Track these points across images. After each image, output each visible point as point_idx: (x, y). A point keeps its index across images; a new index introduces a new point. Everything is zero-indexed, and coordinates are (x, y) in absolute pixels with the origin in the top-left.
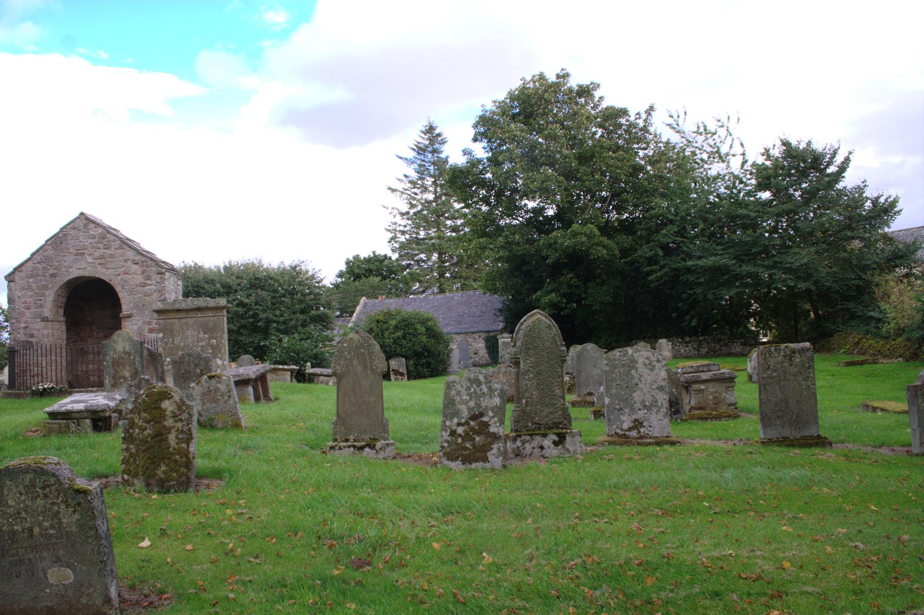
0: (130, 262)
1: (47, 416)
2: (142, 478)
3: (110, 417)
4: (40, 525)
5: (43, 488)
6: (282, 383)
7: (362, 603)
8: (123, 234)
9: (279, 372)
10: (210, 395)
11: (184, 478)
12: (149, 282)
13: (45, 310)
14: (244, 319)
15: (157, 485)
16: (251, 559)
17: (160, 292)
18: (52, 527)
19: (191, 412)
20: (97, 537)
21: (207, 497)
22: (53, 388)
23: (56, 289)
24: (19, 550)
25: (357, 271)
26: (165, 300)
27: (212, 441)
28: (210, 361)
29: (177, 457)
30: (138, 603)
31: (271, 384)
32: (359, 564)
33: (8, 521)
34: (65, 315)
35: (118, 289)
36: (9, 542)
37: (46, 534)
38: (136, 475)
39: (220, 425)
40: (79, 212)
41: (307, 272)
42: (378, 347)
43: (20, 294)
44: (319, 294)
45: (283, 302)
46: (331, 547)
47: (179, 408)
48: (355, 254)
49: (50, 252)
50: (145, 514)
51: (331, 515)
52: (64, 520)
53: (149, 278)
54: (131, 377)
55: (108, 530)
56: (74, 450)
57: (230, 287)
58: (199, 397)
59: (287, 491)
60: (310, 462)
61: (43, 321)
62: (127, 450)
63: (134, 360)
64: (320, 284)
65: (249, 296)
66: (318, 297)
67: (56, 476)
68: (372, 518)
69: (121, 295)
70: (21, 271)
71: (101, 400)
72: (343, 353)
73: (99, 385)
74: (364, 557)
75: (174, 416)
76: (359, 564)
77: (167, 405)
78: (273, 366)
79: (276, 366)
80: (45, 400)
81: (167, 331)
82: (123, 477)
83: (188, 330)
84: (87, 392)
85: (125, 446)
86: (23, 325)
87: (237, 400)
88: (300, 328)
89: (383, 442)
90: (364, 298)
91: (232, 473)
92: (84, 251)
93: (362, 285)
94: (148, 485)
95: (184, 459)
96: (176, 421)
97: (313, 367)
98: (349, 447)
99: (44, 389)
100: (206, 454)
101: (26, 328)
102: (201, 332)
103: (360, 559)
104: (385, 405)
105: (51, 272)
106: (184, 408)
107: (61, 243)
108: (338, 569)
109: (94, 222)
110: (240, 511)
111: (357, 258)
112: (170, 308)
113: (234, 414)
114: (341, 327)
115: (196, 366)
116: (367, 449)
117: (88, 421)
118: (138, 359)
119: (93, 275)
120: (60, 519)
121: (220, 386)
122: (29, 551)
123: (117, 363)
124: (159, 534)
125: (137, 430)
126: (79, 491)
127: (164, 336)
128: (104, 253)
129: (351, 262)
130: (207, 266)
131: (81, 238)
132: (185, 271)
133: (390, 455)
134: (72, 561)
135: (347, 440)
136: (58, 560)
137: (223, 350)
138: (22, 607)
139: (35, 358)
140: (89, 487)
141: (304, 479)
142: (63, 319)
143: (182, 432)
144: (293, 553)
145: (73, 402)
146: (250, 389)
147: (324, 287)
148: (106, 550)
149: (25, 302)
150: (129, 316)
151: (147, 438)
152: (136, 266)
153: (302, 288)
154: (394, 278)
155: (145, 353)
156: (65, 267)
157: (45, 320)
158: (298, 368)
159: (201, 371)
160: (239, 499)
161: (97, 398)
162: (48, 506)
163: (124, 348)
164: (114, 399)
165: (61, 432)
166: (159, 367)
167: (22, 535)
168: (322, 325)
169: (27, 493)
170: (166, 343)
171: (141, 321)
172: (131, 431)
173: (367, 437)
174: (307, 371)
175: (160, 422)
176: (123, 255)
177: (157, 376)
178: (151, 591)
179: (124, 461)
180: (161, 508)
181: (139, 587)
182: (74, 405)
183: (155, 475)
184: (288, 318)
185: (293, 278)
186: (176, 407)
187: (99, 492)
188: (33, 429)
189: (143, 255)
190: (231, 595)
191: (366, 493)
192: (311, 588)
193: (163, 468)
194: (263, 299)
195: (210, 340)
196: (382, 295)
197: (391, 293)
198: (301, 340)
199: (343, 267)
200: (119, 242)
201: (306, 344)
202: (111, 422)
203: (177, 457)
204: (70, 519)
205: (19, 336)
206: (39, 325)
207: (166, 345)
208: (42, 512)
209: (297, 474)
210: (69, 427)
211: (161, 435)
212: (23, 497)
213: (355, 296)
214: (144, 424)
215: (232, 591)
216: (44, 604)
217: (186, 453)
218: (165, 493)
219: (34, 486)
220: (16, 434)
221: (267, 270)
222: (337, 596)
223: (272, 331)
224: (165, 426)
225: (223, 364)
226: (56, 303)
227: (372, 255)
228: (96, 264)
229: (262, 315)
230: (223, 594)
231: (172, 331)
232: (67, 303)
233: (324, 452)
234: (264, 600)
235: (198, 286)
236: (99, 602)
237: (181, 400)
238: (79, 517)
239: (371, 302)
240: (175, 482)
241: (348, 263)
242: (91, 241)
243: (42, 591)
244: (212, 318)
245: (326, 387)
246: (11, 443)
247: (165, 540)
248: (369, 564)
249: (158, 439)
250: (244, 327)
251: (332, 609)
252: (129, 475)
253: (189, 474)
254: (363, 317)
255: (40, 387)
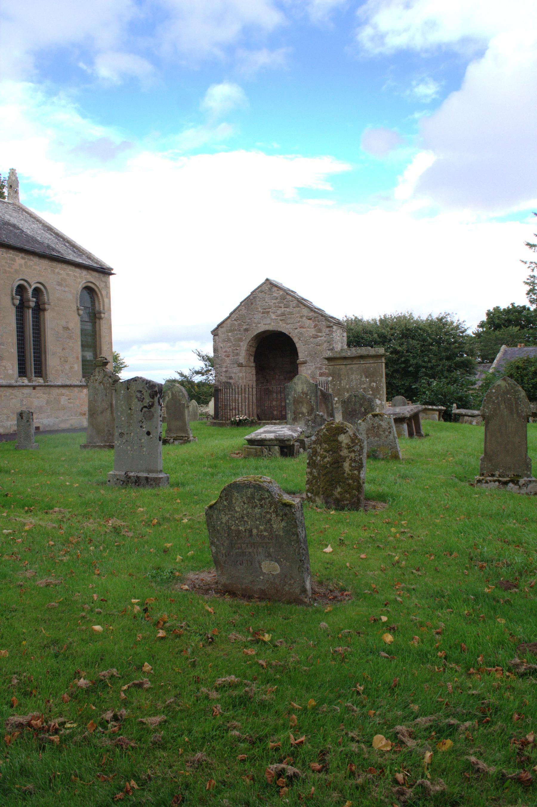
0: (305, 318)
1: (246, 442)
2: (322, 496)
3: (293, 445)
4: (257, 528)
5: (260, 500)
6: (431, 421)
7: (511, 620)
8: (299, 294)
9: (428, 412)
10: (374, 430)
11: (355, 499)
12: (320, 334)
13: (240, 357)
14: (397, 365)
15: (334, 503)
16: (414, 571)
17: (329, 342)
18: (266, 530)
19: (362, 445)
20: (298, 541)
21: (374, 516)
22: (246, 419)
23: (248, 341)
24: (243, 545)
25: (497, 321)
26: (332, 349)
27: (375, 469)
28: (373, 401)
29: (350, 481)
30: (325, 596)
31: (422, 422)
32: (508, 586)
33: (235, 522)
34: (255, 361)
35: (295, 340)
36: (236, 538)
37: (261, 535)
38: (317, 494)
39: (381, 456)
40: (265, 279)
41: (452, 323)
42: (523, 393)
43: (222, 345)
44: (462, 343)
45: (431, 350)
46: (482, 568)
47: (353, 441)
48: (495, 306)
49: (244, 312)
50: (327, 526)
51: (481, 540)
52: (274, 526)
53: (320, 331)
54: (308, 413)
55: (305, 536)
56: (268, 470)
57: (385, 337)
58: (365, 432)
59: (442, 516)
60: (460, 492)
61: (239, 366)
62: (311, 473)
63: (310, 399)
64: (464, 334)
65: (401, 345)
66: (462, 346)
67: (270, 492)
68: (518, 546)
69: (297, 345)
70: (223, 327)
71: (287, 432)
72: (491, 398)
73: (282, 418)
74: (511, 580)
75: (349, 447)
76: (508, 586)
77: (343, 438)
78: (424, 407)
79: (426, 406)
80: (241, 429)
81: (336, 375)
82: (307, 495)
83: (352, 374)
84: (272, 424)
85: (309, 470)
86: (224, 370)
87: (396, 435)
88: (446, 373)
89: (526, 479)
90: (504, 347)
91: (394, 497)
92: (269, 310)
93: (502, 334)
94: (327, 503)
95: (356, 483)
96: (350, 452)
97: (458, 408)
98: (495, 481)
99: (240, 420)
100: (372, 480)
101: (226, 371)
102: (363, 376)
103: (508, 581)
104: (529, 445)
105: (245, 327)
106: (357, 441)
107: (252, 304)
108: (489, 588)
109: (276, 286)
110: (402, 530)
111: (497, 309)
112: (338, 356)
113: (394, 447)
114: (482, 372)
115: (361, 405)
116: (511, 485)
117: (277, 447)
118: (313, 398)
119: (276, 329)
120: (271, 525)
121: (382, 423)
122: (249, 546)
123: (297, 402)
124: (338, 543)
125: (319, 458)
126: (286, 505)
127: (333, 379)
128: (284, 311)
129: (491, 313)
130: (365, 319)
131: (266, 299)
132: (348, 324)
133: (532, 491)
134: (279, 557)
135: (493, 475)
136: (269, 556)
137: (381, 392)
138: (244, 587)
139: (234, 396)
140: (293, 502)
141: (456, 507)
142: (253, 364)
143: (355, 461)
144: (448, 570)
145: (265, 432)
146: (405, 426)
147: (468, 336)
148: (304, 552)
149: (226, 352)
150: (304, 363)
151: (327, 464)
152: (309, 321)
153: (447, 337)
154: (531, 328)
155: (319, 393)
156: (255, 323)
157: (240, 365)
158: (445, 408)
159: (365, 410)
160: (401, 520)
161: (283, 429)
162: (263, 514)
163: (303, 389)
164: (297, 431)
165: (258, 455)
166: (330, 404)
167: (244, 533)
168: (466, 370)
169: (248, 503)
170: (335, 385)
171: (314, 366)
172: (314, 458)
173: (511, 474)
174: (453, 412)
175: (337, 452)
176: (299, 312)
177: (328, 412)
178: (335, 587)
179: (308, 482)
180: (339, 522)
181: (326, 584)
182: (266, 435)
183: (333, 495)
184: (435, 364)
185: (440, 329)
186: (350, 440)
187: (300, 507)
188: (237, 452)
189: (315, 312)
190: (399, 599)
191: (511, 524)
192: (466, 601)
193: (339, 490)
194: (414, 347)
195: (370, 384)
196: (521, 343)
197: (529, 342)
198: (448, 384)
199: (485, 318)
200: (296, 302)
201: (452, 388)
202: (294, 449)
203: (350, 481)
204: (278, 525)
205: (221, 378)
206: (236, 369)
207: (334, 387)
208: (259, 518)
209: (450, 503)
210: (263, 452)
211: (338, 463)
212: (246, 506)
213: (496, 344)
214: (324, 453)
215: (399, 595)
216: (259, 587)
217: (357, 479)
218: (340, 510)
219: (254, 498)
220: (225, 455)
221: (416, 322)
222: (489, 611)
223: (420, 374)
224: (341, 456)
225: (381, 404)
226: (248, 352)
227: (511, 307)
228: (278, 320)
229: (413, 361)
230: (393, 597)
231: (339, 375)
232: (256, 352)
233: (472, 485)
234: (426, 606)
235: (358, 337)
236: (298, 591)
237: (354, 434)
238: (286, 525)
239: (510, 349)
240: (348, 502)
241: (489, 314)
242: (275, 301)
243: (257, 577)
244: (373, 365)
245: (470, 426)
246: (221, 462)
247: (344, 548)
248: (516, 586)
249: (336, 465)
250: (397, 371)
251: (484, 621)
252: (312, 493)
253: (360, 496)
254: (503, 363)
255: (237, 419)
